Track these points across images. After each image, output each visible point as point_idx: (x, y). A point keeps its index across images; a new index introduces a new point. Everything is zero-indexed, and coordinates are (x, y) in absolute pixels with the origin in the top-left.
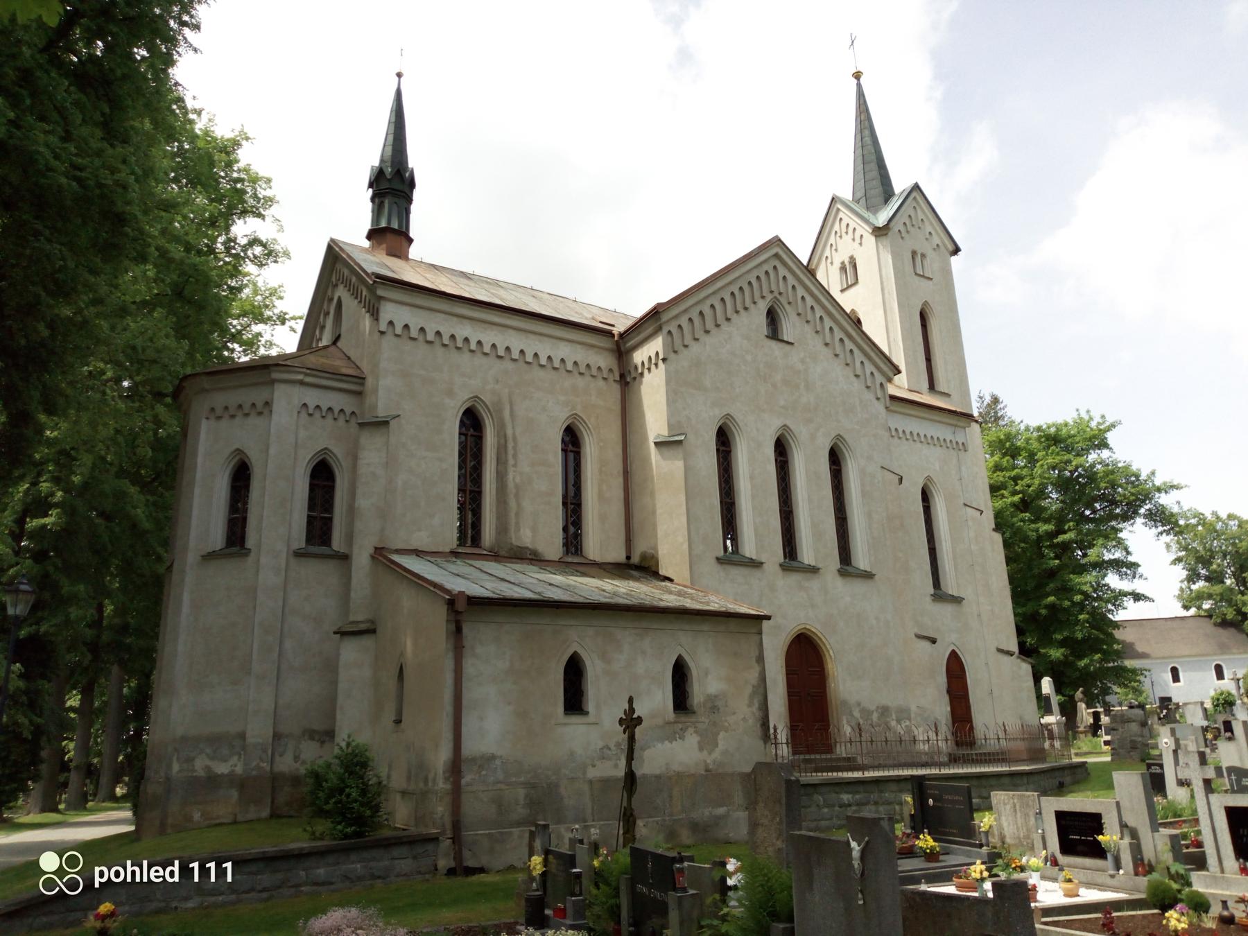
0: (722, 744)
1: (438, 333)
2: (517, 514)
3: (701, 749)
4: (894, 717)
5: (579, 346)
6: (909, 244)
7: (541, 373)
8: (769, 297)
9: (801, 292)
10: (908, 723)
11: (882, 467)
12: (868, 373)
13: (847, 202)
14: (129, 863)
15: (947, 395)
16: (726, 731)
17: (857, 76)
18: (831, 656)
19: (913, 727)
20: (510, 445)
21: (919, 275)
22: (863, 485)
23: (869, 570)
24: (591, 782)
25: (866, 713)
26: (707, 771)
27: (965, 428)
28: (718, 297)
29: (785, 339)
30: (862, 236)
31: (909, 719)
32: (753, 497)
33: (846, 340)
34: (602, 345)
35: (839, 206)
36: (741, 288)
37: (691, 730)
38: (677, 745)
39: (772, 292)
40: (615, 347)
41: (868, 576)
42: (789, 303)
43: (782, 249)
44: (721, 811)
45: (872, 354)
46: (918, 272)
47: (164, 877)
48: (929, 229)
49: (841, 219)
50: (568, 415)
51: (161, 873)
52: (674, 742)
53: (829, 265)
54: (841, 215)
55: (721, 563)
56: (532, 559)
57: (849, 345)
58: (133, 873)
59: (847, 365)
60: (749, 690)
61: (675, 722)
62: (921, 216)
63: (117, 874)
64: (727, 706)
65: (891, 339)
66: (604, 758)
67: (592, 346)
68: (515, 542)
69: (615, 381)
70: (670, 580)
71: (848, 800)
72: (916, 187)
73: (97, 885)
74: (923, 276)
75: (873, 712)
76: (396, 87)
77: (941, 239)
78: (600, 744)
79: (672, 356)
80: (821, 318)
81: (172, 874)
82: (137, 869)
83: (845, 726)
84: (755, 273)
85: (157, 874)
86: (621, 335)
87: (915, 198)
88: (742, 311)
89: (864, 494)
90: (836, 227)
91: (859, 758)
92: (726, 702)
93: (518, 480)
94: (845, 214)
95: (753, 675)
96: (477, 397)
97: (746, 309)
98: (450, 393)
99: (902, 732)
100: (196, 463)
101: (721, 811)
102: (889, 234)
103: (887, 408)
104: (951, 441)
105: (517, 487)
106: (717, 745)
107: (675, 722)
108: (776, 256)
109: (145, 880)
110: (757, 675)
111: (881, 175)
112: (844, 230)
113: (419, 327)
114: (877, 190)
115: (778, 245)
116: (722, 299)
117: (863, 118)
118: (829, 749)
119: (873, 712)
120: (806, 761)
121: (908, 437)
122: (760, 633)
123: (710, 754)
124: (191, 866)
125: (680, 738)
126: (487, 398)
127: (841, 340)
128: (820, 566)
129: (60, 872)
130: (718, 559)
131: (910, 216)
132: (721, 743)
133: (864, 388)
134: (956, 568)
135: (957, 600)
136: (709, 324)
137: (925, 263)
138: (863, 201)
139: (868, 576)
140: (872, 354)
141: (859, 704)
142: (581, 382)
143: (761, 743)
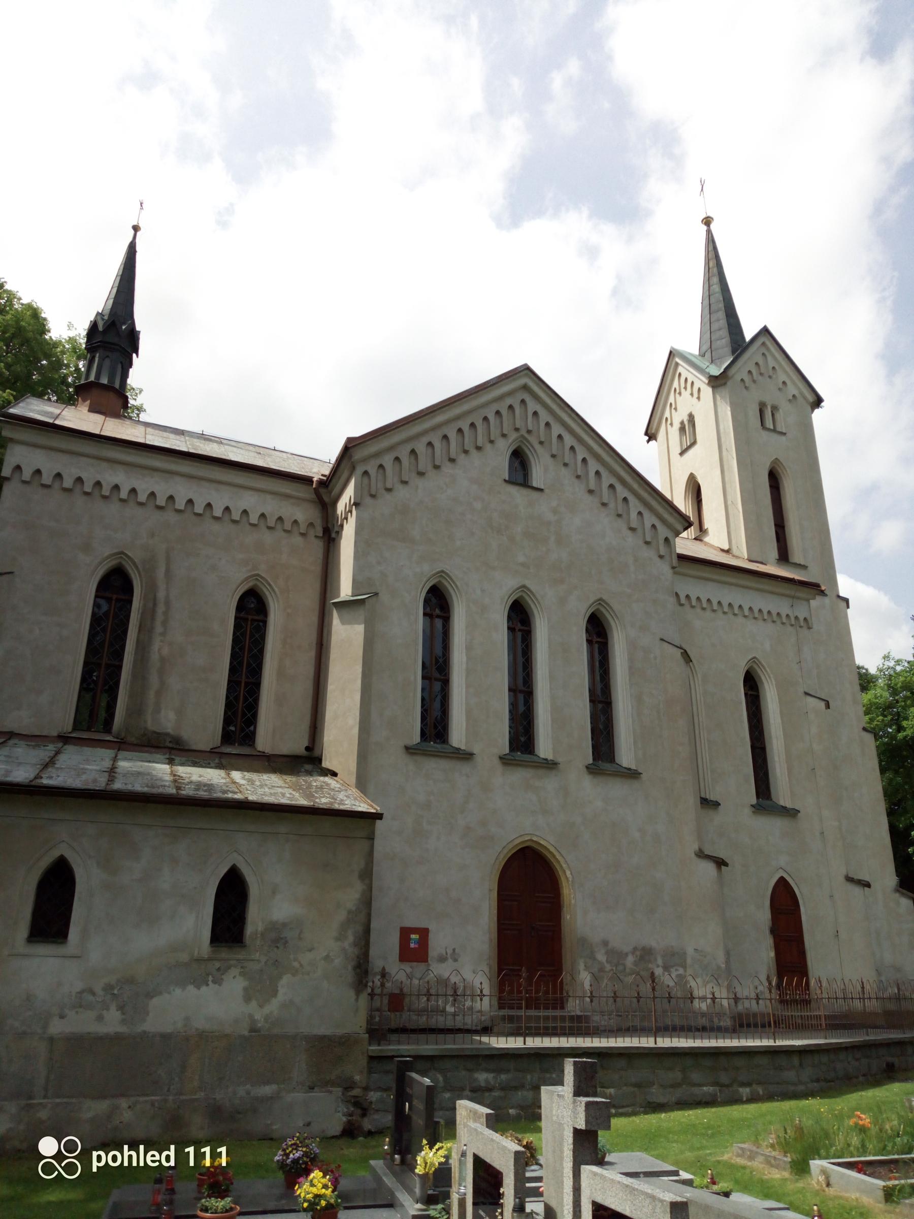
0: (283, 993)
1: (79, 480)
2: (158, 693)
3: (247, 998)
4: (660, 961)
5: (269, 497)
6: (754, 396)
7: (216, 527)
8: (513, 436)
9: (557, 429)
10: (681, 971)
11: (662, 640)
12: (648, 525)
13: (693, 359)
14: (126, 1147)
15: (804, 567)
16: (294, 975)
17: (707, 221)
18: (567, 878)
19: (690, 979)
20: (161, 609)
21: (769, 430)
22: (631, 660)
23: (633, 767)
24: (51, 1040)
25: (616, 956)
26: (253, 1030)
27: (808, 600)
28: (440, 433)
29: (535, 485)
30: (699, 390)
31: (685, 967)
32: (468, 672)
33: (619, 487)
34: (301, 495)
35: (677, 360)
36: (473, 425)
37: (234, 971)
38: (208, 991)
39: (517, 430)
40: (314, 496)
41: (632, 775)
42: (541, 443)
43: (530, 378)
44: (267, 1090)
45: (654, 503)
46: (768, 426)
47: (160, 1161)
48: (782, 377)
49: (680, 374)
50: (246, 576)
51: (157, 1158)
52: (204, 988)
53: (669, 426)
54: (680, 369)
55: (412, 754)
56: (172, 748)
57: (622, 492)
58: (130, 1157)
59: (619, 516)
60: (341, 916)
61: (210, 959)
62: (771, 363)
63: (114, 1159)
64: (300, 939)
65: (729, 502)
66: (81, 1006)
67: (287, 496)
68: (151, 725)
69: (316, 537)
70: (334, 774)
71: (487, 1081)
72: (765, 331)
74: (774, 430)
75: (627, 954)
76: (130, 239)
77: (799, 388)
78: (79, 986)
79: (368, 500)
80: (584, 460)
81: (168, 1158)
82: (133, 1153)
83: (582, 972)
84: (495, 407)
85: (153, 1159)
86: (321, 483)
87: (764, 344)
88: (473, 452)
89: (632, 670)
90: (676, 384)
91: (596, 1018)
92: (301, 932)
93: (165, 651)
94: (685, 370)
95: (351, 896)
96: (122, 553)
97: (479, 448)
98: (87, 548)
99: (672, 984)
101: (267, 1090)
102: (728, 383)
103: (673, 568)
104: (787, 615)
105: (163, 660)
106: (275, 993)
107: (210, 959)
108: (525, 387)
109: (142, 1164)
110: (357, 896)
111: (729, 325)
112: (683, 385)
113: (55, 472)
114: (724, 341)
115: (526, 375)
116: (445, 437)
117: (711, 265)
118: (560, 1003)
119: (627, 954)
120: (511, 1019)
121: (705, 605)
122: (371, 838)
123: (261, 1006)
124: (187, 1150)
125: (214, 982)
126: (137, 555)
127: (611, 486)
128: (559, 759)
129: (59, 1156)
130: (407, 748)
131: (757, 364)
132: (281, 991)
133: (641, 542)
134: (790, 770)
135: (791, 813)
136: (424, 462)
137: (777, 416)
138: (708, 355)
139: (632, 775)
140: (654, 503)
141: (605, 943)
142: (268, 538)
143: (352, 994)
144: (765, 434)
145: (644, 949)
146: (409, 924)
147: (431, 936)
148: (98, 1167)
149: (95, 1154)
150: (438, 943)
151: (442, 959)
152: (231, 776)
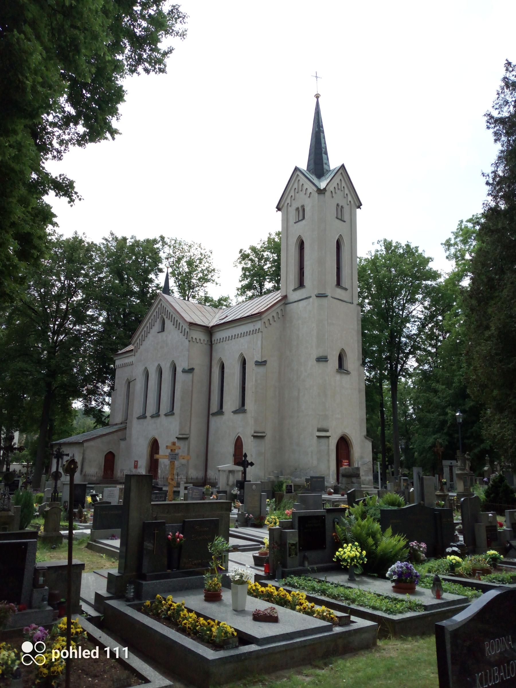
47: (90, 655)
49: (299, 180)
51: (89, 653)
58: (74, 653)
63: (65, 654)
73: (53, 660)
74: (341, 220)
81: (95, 654)
82: (75, 651)
85: (87, 654)
90: (296, 186)
100: (391, 566)
109: (80, 657)
129: (33, 653)
144: (338, 221)
148: (55, 659)
152: (389, 582)
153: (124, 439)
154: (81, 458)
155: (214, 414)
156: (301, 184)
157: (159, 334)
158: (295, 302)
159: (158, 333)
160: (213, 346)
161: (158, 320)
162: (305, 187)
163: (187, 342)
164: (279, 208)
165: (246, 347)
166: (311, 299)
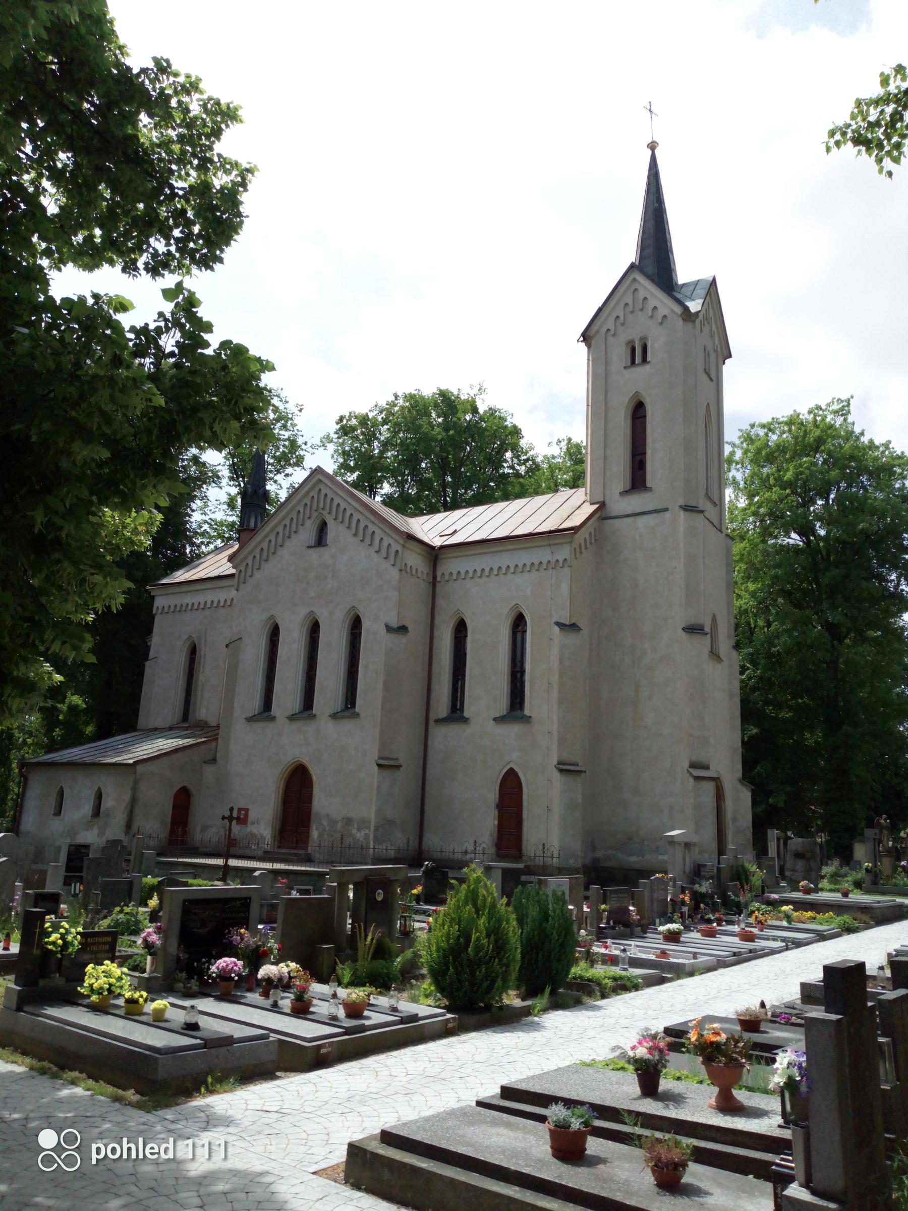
4: (356, 826)
14: (125, 1140)
25: (332, 822)
47: (159, 1153)
51: (156, 1150)
58: (129, 1149)
63: (114, 1150)
73: (94, 1162)
82: (133, 1146)
85: (152, 1151)
109: (141, 1156)
122: (135, 773)
129: (58, 1149)
141: (328, 815)
145: (348, 818)
146: (241, 806)
147: (250, 812)
148: (97, 1160)
149: (94, 1147)
150: (252, 815)
151: (253, 823)
153: (213, 761)
154: (127, 797)
155: (437, 721)
156: (641, 297)
157: (311, 551)
158: (628, 516)
159: (308, 547)
160: (438, 585)
161: (308, 523)
162: (652, 303)
163: (395, 573)
164: (586, 337)
165: (529, 592)
166: (667, 515)
